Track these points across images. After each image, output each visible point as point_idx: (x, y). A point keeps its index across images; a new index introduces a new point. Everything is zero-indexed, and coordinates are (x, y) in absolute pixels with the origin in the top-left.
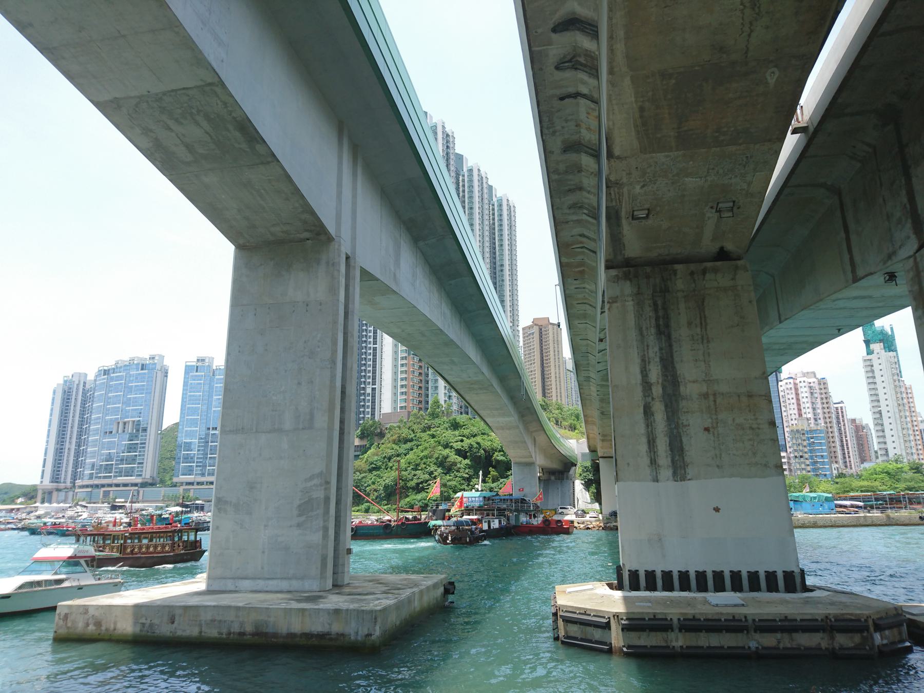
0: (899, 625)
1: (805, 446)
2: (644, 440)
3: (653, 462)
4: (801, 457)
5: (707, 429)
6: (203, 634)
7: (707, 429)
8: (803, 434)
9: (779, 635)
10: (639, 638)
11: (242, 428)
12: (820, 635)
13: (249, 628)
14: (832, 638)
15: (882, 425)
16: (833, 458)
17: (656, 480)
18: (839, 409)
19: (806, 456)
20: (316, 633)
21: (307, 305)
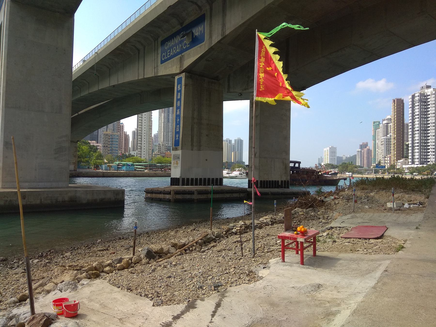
0: (245, 192)
1: (109, 142)
2: (190, 137)
3: (192, 145)
4: (107, 146)
5: (207, 135)
6: (42, 203)
7: (207, 135)
8: (109, 136)
9: (230, 194)
10: (201, 196)
11: (20, 107)
12: (237, 194)
13: (67, 199)
14: (240, 195)
15: (141, 136)
16: (120, 148)
17: (192, 150)
18: (122, 126)
19: (109, 146)
20: (84, 202)
21: (57, 49)
